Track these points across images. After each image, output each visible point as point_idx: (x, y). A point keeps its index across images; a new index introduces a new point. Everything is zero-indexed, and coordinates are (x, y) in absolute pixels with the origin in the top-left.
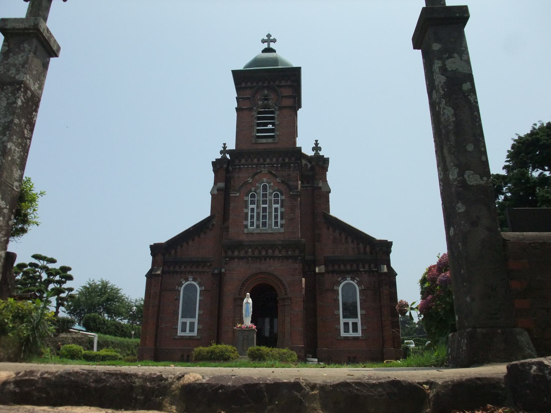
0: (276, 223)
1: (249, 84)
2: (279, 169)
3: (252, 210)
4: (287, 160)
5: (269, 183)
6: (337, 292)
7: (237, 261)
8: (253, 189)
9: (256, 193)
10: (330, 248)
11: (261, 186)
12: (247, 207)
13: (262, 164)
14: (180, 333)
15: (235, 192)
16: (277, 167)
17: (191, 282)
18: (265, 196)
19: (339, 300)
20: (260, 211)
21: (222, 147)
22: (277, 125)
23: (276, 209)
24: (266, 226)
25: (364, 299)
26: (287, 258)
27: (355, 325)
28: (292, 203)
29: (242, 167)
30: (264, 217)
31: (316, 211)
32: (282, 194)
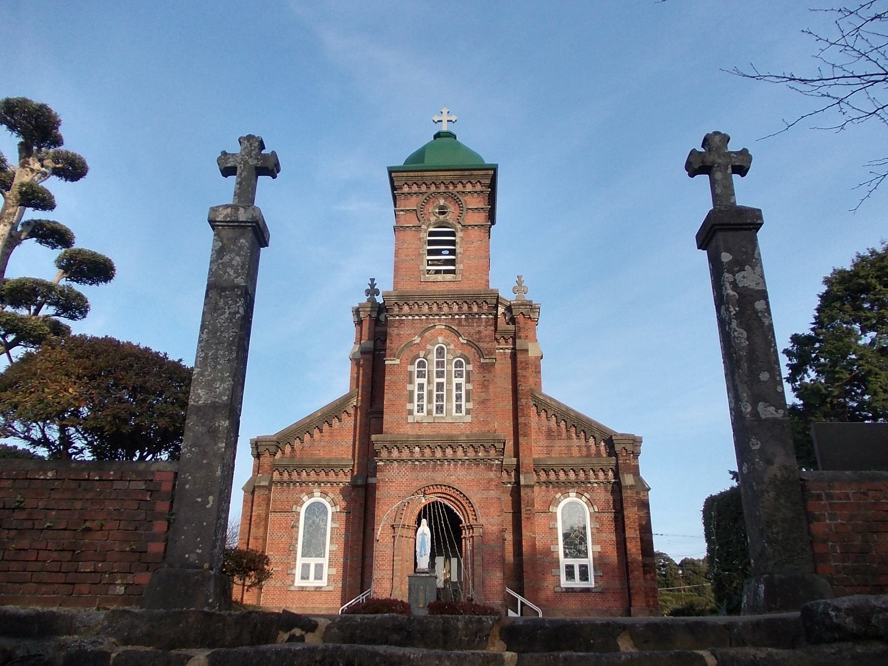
0: (459, 408)
2: (464, 323)
3: (421, 387)
4: (475, 309)
5: (447, 345)
6: (553, 517)
8: (422, 354)
11: (433, 349)
12: (411, 382)
13: (437, 315)
14: (299, 582)
17: (317, 498)
18: (440, 364)
22: (460, 253)
23: (459, 387)
24: (442, 412)
26: (476, 461)
27: (584, 570)
28: (484, 377)
29: (404, 320)
30: (440, 397)
31: (520, 388)
32: (468, 363)
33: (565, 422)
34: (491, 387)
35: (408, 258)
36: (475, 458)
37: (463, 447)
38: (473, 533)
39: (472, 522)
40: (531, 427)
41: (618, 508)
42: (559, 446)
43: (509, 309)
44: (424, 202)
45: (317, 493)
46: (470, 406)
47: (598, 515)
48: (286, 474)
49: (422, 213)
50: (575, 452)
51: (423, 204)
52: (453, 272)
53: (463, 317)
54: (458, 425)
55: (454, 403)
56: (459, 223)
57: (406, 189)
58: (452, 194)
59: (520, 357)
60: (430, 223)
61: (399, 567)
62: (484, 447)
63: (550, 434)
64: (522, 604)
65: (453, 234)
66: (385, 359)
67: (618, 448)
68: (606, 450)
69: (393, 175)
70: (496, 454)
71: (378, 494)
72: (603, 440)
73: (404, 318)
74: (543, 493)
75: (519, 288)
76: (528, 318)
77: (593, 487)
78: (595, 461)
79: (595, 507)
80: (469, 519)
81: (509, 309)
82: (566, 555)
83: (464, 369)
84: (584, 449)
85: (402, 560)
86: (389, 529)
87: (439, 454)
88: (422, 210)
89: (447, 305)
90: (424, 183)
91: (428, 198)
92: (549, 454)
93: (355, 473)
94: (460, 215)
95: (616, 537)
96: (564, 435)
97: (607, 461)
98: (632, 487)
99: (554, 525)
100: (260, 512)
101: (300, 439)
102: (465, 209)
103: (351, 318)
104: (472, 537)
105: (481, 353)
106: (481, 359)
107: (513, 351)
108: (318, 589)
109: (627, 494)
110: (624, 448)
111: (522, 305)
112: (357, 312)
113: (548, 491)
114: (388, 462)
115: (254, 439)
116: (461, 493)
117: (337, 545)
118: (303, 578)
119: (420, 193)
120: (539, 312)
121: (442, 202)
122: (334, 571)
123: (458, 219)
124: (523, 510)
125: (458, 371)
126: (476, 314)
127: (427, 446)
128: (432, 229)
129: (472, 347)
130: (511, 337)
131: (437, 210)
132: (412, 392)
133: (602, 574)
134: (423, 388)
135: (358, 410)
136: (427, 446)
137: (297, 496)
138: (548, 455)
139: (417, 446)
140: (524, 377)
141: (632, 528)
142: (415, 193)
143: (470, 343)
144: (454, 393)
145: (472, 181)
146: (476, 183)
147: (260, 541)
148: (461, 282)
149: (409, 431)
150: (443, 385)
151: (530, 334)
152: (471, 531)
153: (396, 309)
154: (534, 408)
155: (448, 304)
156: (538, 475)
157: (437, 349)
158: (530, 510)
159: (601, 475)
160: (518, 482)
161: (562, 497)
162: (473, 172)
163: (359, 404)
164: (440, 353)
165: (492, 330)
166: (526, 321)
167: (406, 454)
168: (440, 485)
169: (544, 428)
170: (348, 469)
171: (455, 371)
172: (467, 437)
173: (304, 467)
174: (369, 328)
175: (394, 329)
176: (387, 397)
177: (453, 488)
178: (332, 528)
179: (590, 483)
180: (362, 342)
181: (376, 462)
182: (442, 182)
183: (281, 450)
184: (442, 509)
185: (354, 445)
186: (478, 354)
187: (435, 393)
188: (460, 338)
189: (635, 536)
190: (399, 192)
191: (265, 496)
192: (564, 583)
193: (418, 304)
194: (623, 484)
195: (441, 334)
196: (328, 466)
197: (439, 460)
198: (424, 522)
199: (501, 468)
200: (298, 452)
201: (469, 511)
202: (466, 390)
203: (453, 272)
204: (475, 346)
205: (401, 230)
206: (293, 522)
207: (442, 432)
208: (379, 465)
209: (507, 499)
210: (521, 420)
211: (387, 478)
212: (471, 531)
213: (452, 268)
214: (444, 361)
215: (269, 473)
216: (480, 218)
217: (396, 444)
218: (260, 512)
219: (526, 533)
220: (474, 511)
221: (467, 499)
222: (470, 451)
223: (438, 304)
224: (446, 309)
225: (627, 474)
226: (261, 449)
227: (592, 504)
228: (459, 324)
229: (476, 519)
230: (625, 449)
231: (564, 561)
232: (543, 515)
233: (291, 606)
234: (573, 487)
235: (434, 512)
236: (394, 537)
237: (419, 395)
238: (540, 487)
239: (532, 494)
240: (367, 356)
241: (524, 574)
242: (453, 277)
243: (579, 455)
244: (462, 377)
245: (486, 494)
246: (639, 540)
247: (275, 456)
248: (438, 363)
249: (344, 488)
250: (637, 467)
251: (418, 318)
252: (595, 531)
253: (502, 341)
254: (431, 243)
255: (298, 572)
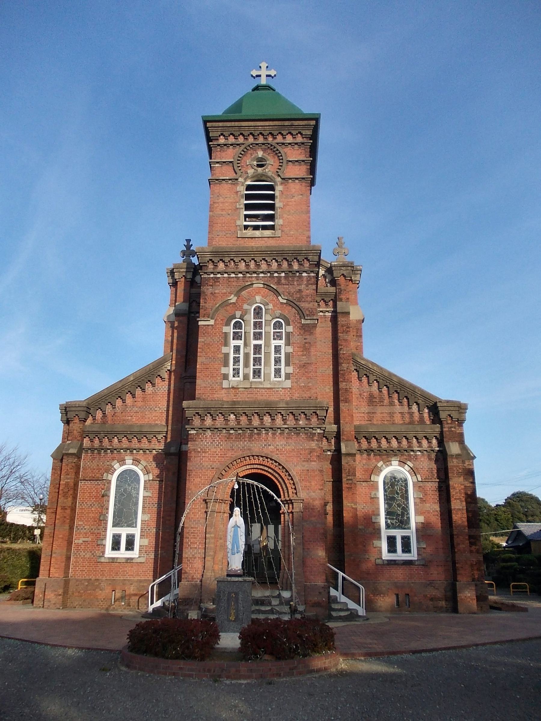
0: (278, 372)
1: (231, 140)
2: (283, 281)
3: (237, 349)
4: (296, 266)
5: (266, 304)
6: (375, 486)
7: (211, 436)
8: (238, 314)
9: (243, 321)
10: (364, 413)
11: (250, 309)
12: (226, 344)
13: (255, 272)
14: (109, 553)
15: (208, 319)
16: (279, 278)
17: (129, 465)
18: (257, 325)
19: (378, 498)
20: (250, 350)
21: (184, 245)
22: (280, 208)
23: (278, 349)
24: (259, 376)
25: (421, 498)
26: (296, 430)
27: (406, 541)
28: (305, 339)
29: (219, 278)
30: (257, 361)
31: (341, 352)
32: (287, 324)
33: (388, 387)
34: (312, 350)
35: (224, 213)
36: (295, 426)
37: (282, 415)
38: (293, 508)
39: (292, 496)
40: (352, 392)
41: (443, 477)
42: (381, 412)
43: (330, 270)
44: (241, 154)
45: (129, 461)
46: (290, 370)
47: (421, 484)
48: (97, 441)
49: (239, 165)
50: (398, 419)
51: (241, 156)
52: (272, 228)
53: (283, 275)
54: (277, 391)
55: (273, 367)
56: (279, 176)
57: (222, 140)
58: (272, 146)
59: (341, 320)
60: (248, 177)
61: (212, 546)
62: (306, 415)
63: (371, 400)
64: (344, 578)
65: (271, 188)
66: (199, 319)
67: (443, 415)
68: (429, 417)
69: (208, 125)
70: (318, 422)
71: (190, 465)
72: (427, 406)
73: (219, 276)
74: (364, 462)
75: (339, 250)
76: (350, 280)
77: (416, 455)
78: (418, 428)
79: (419, 476)
80: (288, 492)
81: (330, 270)
82: (388, 526)
83: (284, 331)
84: (407, 416)
85: (215, 538)
86: (201, 504)
87: (256, 422)
88: (239, 162)
89: (265, 262)
90: (242, 134)
91: (245, 150)
92: (370, 421)
93: (169, 440)
94: (280, 167)
95: (440, 507)
96: (386, 401)
97: (431, 429)
98: (458, 456)
99: (375, 494)
100: (69, 481)
101: (112, 404)
102: (285, 162)
103: (166, 280)
104: (292, 513)
105: (301, 313)
106: (302, 320)
107: (334, 314)
108: (129, 560)
109: (452, 463)
110: (450, 415)
111: (344, 266)
112: (172, 273)
113: (369, 459)
114: (201, 431)
115: (63, 405)
116: (280, 464)
117: (149, 515)
118: (113, 549)
119: (238, 145)
120: (360, 274)
121: (260, 154)
122: (146, 542)
123: (277, 172)
124: (344, 480)
125: (277, 332)
126: (297, 272)
127: (243, 413)
128: (249, 183)
129: (293, 307)
130: (331, 299)
131: (255, 163)
132: (227, 355)
133: (425, 546)
134: (239, 350)
135: (173, 374)
136: (243, 413)
137: (108, 463)
138: (369, 422)
139: (232, 413)
140: (346, 340)
141: (458, 499)
142: (231, 145)
143: (290, 303)
144: (273, 355)
145: (292, 132)
146: (297, 134)
147: (68, 511)
148: (281, 238)
149: (223, 396)
150: (261, 348)
151: (352, 297)
152: (291, 506)
153: (211, 266)
154: (355, 373)
155: (266, 261)
156: (359, 443)
157: (255, 309)
158: (351, 480)
159: (425, 443)
160: (338, 449)
161: (384, 465)
162: (294, 122)
163: (173, 368)
164: (258, 313)
165: (313, 290)
166: (347, 284)
167: (220, 421)
168: (257, 456)
169: (365, 394)
170: (161, 436)
171: (274, 332)
172: (287, 403)
173: (116, 434)
174: (184, 290)
175: (208, 287)
176: (201, 360)
177: (271, 459)
178: (144, 497)
179: (413, 451)
180: (177, 304)
181: (188, 431)
182: (261, 133)
183: (92, 415)
184: (259, 495)
185: (168, 411)
186: (298, 313)
187: (252, 356)
188: (280, 298)
189: (461, 507)
190: (215, 143)
191: (73, 464)
192: (386, 555)
193: (234, 261)
194: (449, 453)
195: (258, 293)
196: (141, 432)
197: (256, 428)
198: (237, 510)
199: (324, 436)
200: (109, 418)
201: (288, 485)
202: (286, 353)
203: (272, 228)
204: (295, 306)
205: (216, 184)
206: (103, 491)
207: (260, 398)
208: (191, 434)
209: (327, 467)
210: (342, 385)
211: (200, 447)
212: (291, 506)
213: (271, 223)
214: (262, 322)
215: (79, 440)
216: (301, 171)
217: (209, 411)
218: (69, 481)
219: (347, 504)
220: (294, 484)
221: (287, 471)
222: (290, 419)
223: (255, 261)
224: (264, 266)
225: (452, 442)
226: (71, 415)
227: (415, 473)
228: (279, 282)
229: (296, 493)
230: (450, 416)
231: (385, 533)
232: (364, 484)
233: (101, 578)
234: (396, 455)
235: (250, 498)
236: (206, 512)
237: (234, 358)
238: (361, 455)
239: (354, 463)
240: (181, 318)
241: (345, 547)
242: (272, 233)
243: (401, 422)
244: (281, 339)
245: (306, 466)
246: (465, 511)
247: (85, 422)
248: (255, 324)
249: (156, 455)
250: (461, 435)
251: (234, 276)
252: (418, 501)
253: (322, 303)
254: (248, 197)
255: (109, 542)
